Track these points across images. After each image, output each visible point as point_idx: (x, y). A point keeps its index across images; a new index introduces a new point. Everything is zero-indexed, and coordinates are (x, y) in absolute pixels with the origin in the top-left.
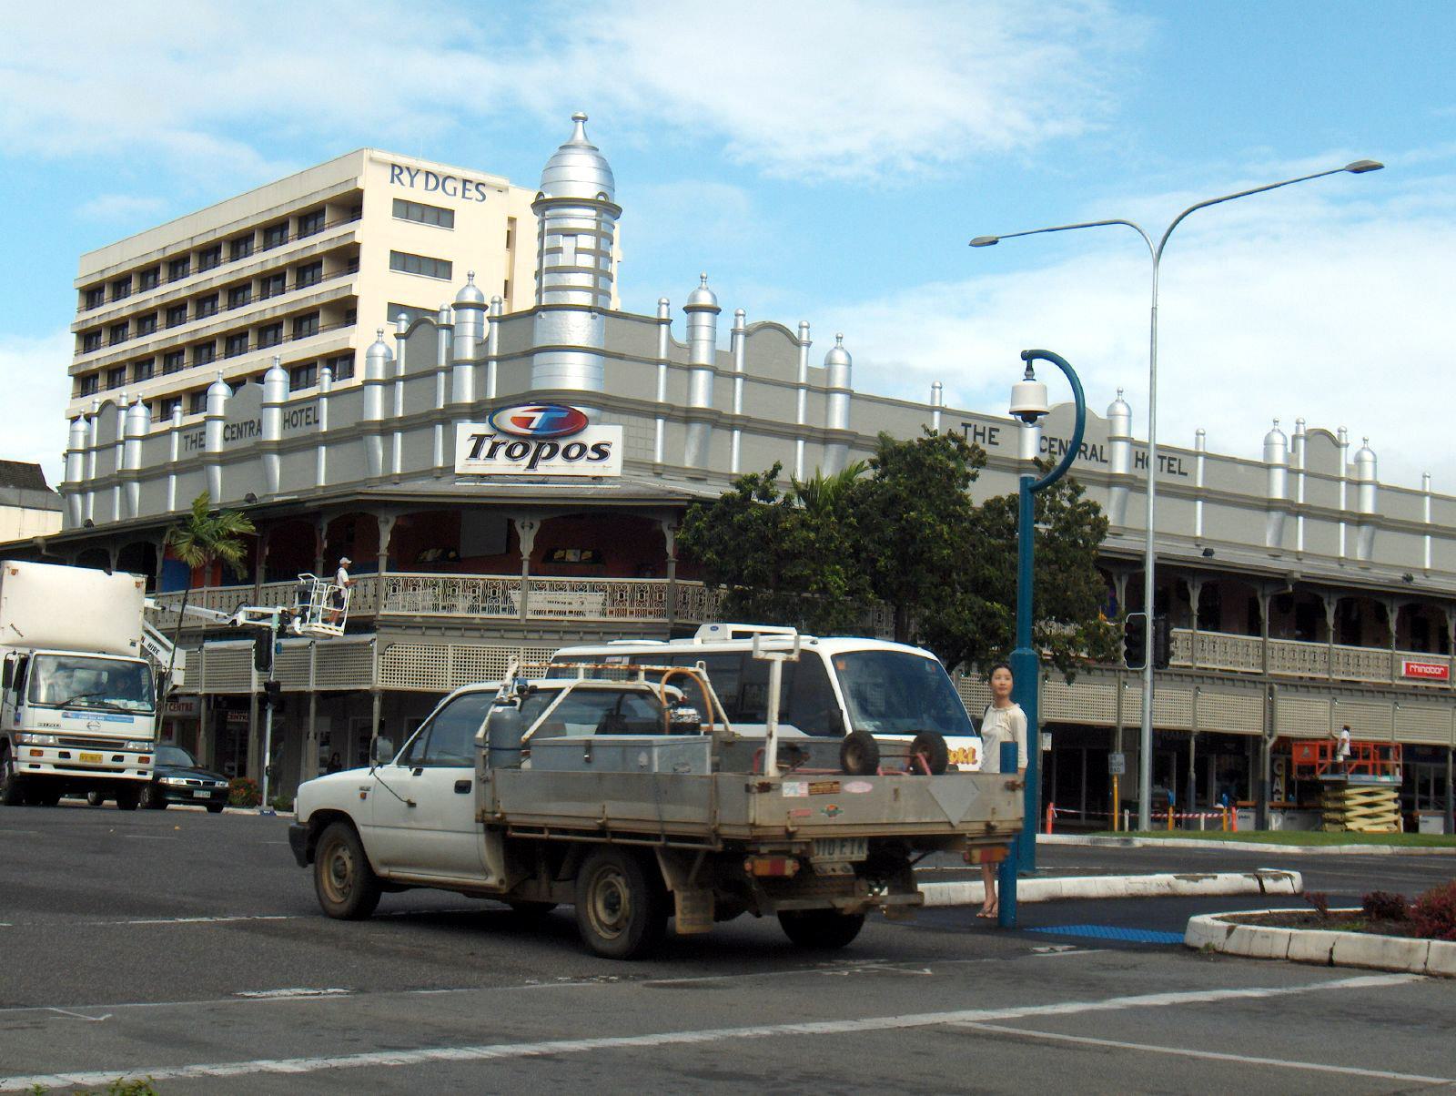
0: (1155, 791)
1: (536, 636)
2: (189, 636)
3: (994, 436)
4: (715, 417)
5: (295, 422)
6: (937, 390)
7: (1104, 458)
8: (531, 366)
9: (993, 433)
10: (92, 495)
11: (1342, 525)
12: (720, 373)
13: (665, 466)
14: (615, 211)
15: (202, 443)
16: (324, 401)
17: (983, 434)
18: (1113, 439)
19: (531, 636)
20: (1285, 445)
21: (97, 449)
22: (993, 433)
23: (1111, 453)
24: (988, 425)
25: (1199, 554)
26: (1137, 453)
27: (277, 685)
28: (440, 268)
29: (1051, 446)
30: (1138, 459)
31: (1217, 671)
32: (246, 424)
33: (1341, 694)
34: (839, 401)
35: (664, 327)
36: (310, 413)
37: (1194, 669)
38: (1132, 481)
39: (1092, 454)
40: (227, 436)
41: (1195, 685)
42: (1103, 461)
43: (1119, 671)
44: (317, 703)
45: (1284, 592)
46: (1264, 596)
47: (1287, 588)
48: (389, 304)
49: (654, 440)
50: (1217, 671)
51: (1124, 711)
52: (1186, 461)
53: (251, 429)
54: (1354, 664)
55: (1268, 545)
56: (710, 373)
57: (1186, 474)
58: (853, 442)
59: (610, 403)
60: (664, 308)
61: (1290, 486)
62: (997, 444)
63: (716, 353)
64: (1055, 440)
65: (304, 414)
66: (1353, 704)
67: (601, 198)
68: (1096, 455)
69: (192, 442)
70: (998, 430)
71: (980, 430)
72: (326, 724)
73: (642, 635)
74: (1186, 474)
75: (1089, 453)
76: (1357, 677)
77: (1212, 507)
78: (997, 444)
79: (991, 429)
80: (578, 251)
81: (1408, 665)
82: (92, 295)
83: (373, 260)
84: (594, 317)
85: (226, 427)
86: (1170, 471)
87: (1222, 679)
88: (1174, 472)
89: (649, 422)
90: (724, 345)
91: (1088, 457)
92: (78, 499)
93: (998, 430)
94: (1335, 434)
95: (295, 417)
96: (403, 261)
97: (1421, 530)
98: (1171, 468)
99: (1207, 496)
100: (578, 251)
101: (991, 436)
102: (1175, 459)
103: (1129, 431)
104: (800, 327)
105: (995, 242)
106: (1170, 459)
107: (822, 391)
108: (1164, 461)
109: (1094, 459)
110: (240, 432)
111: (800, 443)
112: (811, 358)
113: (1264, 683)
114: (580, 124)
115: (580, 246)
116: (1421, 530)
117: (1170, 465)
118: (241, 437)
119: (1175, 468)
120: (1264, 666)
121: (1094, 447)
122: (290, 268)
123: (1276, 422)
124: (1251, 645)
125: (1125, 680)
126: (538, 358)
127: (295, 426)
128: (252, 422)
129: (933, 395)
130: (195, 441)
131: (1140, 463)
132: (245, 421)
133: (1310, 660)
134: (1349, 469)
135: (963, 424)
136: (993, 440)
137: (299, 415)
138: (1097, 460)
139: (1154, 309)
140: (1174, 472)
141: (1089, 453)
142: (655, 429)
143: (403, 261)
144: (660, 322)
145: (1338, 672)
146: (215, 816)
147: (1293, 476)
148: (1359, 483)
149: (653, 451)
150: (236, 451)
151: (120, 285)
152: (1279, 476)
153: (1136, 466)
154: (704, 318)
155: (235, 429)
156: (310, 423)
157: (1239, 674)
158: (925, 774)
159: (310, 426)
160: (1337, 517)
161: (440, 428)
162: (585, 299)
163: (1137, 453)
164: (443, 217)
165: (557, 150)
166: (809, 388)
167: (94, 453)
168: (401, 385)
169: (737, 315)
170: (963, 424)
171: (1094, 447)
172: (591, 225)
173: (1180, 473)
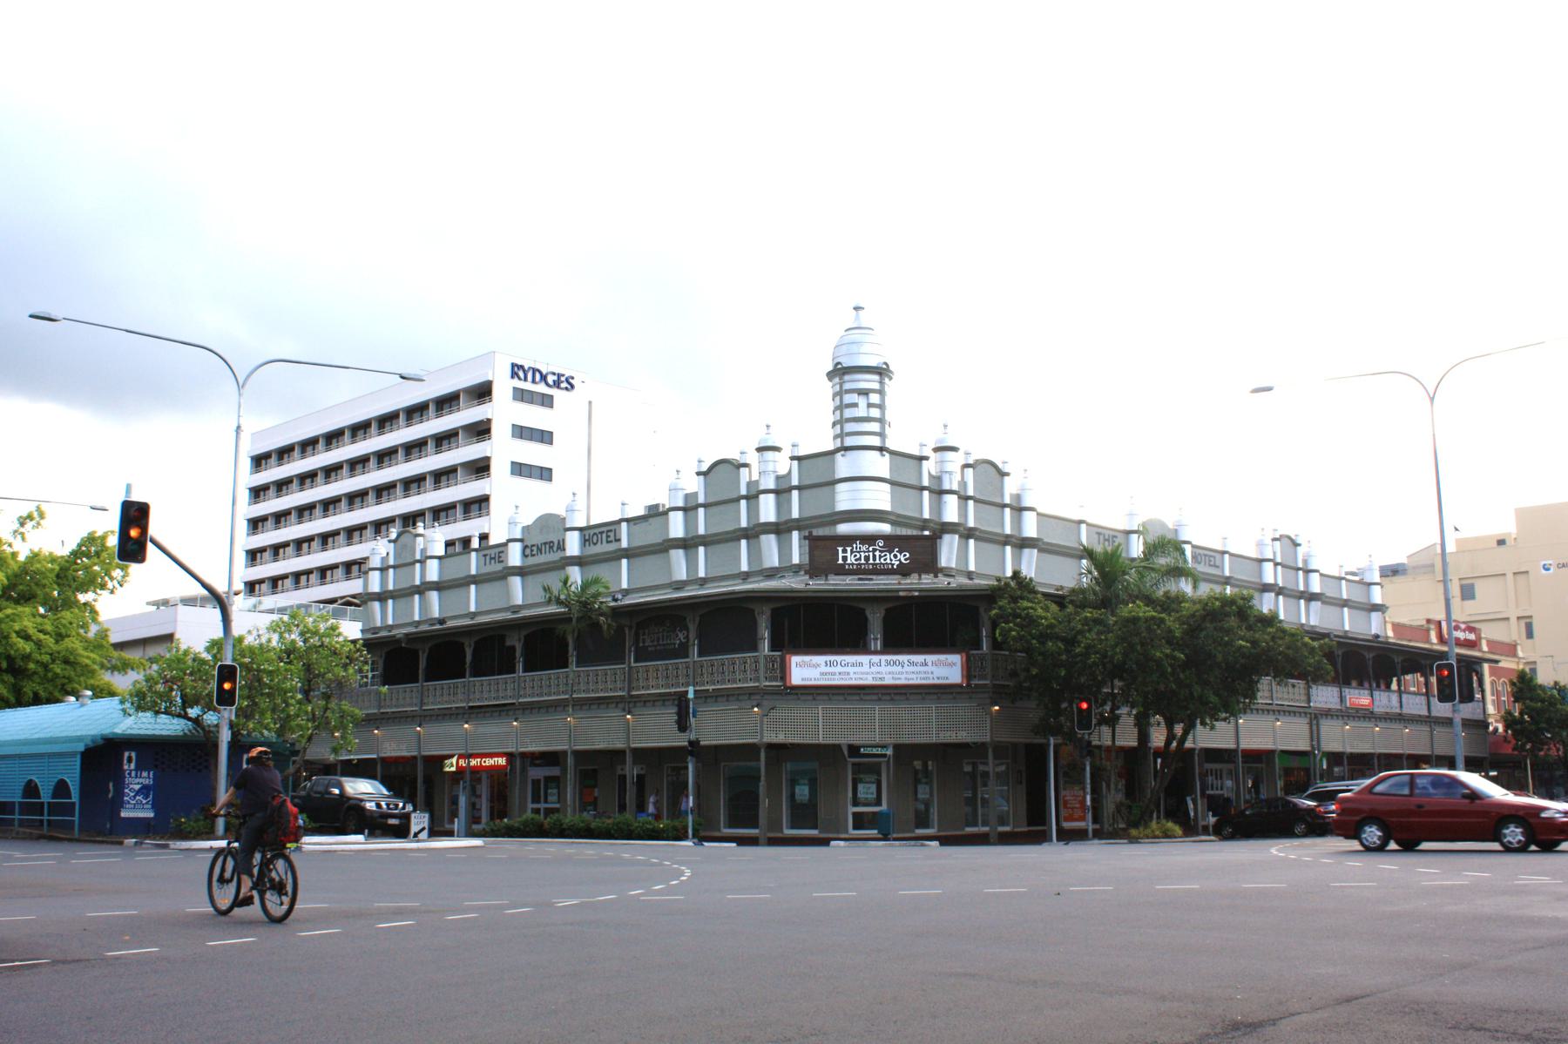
1: (888, 697)
2: (547, 707)
5: (595, 541)
8: (833, 493)
10: (390, 602)
13: (957, 570)
15: (501, 559)
16: (624, 525)
17: (494, 558)
19: (884, 697)
21: (394, 567)
24: (1111, 533)
27: (698, 742)
28: (545, 437)
32: (545, 543)
36: (612, 534)
40: (526, 554)
44: (766, 753)
48: (512, 463)
51: (1435, 746)
53: (551, 547)
65: (604, 535)
66: (722, 710)
69: (491, 559)
70: (503, 552)
71: (493, 556)
72: (344, 752)
81: (1350, 698)
82: (259, 461)
83: (500, 431)
85: (525, 547)
92: (376, 605)
94: (1293, 537)
95: (595, 537)
96: (521, 432)
100: (870, 405)
107: (1019, 509)
110: (540, 550)
112: (1010, 487)
115: (872, 401)
118: (541, 553)
120: (1309, 701)
122: (431, 439)
126: (840, 487)
127: (595, 544)
128: (552, 542)
130: (494, 558)
132: (545, 541)
133: (602, 681)
137: (599, 536)
139: (1434, 435)
143: (521, 432)
145: (579, 691)
146: (700, 847)
150: (529, 566)
151: (284, 453)
155: (535, 548)
156: (611, 542)
159: (610, 545)
161: (744, 543)
164: (547, 401)
167: (391, 571)
168: (701, 511)
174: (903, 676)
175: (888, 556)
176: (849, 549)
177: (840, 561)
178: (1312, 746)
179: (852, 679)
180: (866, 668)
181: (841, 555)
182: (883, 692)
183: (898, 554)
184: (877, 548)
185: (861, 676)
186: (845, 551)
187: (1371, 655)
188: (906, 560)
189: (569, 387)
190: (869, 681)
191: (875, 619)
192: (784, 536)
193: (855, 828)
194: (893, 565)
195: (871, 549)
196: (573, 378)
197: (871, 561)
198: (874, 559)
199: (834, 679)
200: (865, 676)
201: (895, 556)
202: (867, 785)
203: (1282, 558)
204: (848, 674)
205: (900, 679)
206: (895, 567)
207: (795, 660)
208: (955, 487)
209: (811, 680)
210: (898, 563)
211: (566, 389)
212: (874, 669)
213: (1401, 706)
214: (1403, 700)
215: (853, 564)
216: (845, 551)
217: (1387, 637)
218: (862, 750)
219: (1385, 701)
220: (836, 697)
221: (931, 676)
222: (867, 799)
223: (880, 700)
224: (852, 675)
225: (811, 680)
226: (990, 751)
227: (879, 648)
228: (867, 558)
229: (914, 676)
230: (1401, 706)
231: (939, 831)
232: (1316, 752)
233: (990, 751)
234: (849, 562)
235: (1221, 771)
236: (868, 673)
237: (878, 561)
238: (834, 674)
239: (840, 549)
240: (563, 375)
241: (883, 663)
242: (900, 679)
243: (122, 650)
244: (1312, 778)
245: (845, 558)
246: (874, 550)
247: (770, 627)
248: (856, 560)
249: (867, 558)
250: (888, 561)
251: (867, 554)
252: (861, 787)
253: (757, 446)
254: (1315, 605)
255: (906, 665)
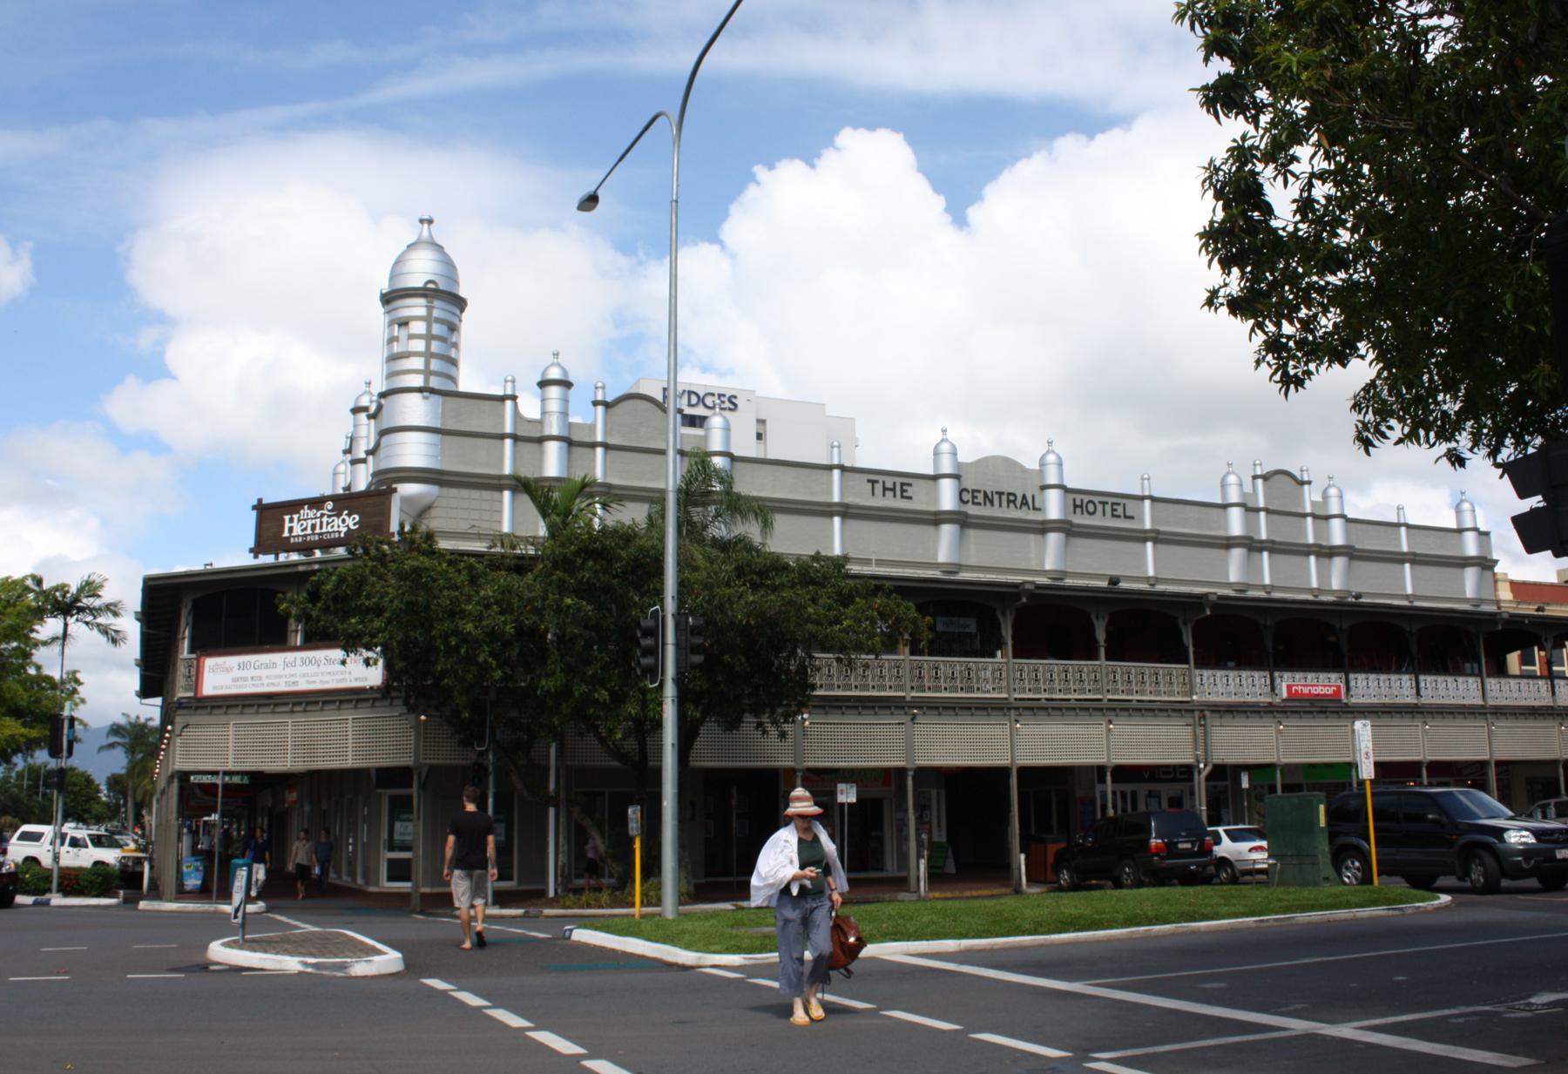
0: (1554, 816)
3: (906, 491)
4: (962, 517)
6: (1146, 482)
7: (1127, 514)
9: (905, 488)
11: (1407, 566)
12: (1249, 509)
14: (460, 303)
18: (1044, 488)
20: (1241, 485)
22: (905, 488)
23: (1043, 501)
24: (1086, 498)
25: (1104, 584)
26: (1074, 500)
29: (974, 497)
30: (1075, 506)
31: (1134, 702)
33: (1117, 715)
34: (1336, 524)
35: (1306, 487)
37: (1105, 701)
38: (1483, 561)
39: (1022, 504)
41: (1107, 719)
42: (1034, 508)
43: (1009, 709)
45: (1202, 616)
46: (1185, 623)
47: (1204, 611)
49: (500, 511)
50: (1043, 701)
52: (1131, 507)
54: (1261, 685)
55: (1048, 567)
56: (565, 445)
57: (1132, 518)
58: (1069, 530)
59: (446, 478)
60: (1305, 474)
61: (1250, 523)
62: (910, 498)
63: (1244, 495)
64: (979, 491)
67: (431, 286)
68: (1027, 504)
70: (910, 485)
73: (209, 710)
74: (1132, 518)
75: (1018, 502)
76: (998, 693)
77: (1419, 568)
78: (910, 498)
79: (902, 484)
80: (411, 337)
84: (425, 398)
86: (1113, 516)
87: (1140, 710)
88: (1119, 516)
89: (495, 494)
90: (1248, 488)
91: (1018, 506)
93: (910, 485)
97: (1399, 559)
98: (976, 500)
99: (1158, 537)
100: (411, 337)
101: (903, 491)
102: (1118, 504)
103: (1342, 506)
104: (1302, 471)
105: (409, 246)
106: (1113, 504)
107: (1323, 518)
108: (876, 485)
109: (1025, 508)
111: (1312, 558)
113: (1193, 711)
114: (426, 226)
116: (1399, 559)
117: (1113, 510)
119: (1120, 511)
121: (1024, 497)
123: (1462, 493)
124: (1174, 673)
125: (1018, 718)
129: (1398, 515)
131: (1078, 510)
134: (1313, 503)
135: (869, 481)
136: (905, 494)
138: (895, 496)
140: (1119, 516)
141: (1018, 502)
142: (501, 502)
144: (502, 399)
147: (1323, 522)
148: (1328, 518)
149: (500, 522)
152: (1235, 515)
153: (1075, 512)
154: (554, 391)
157: (1043, 701)
158: (87, 847)
160: (1304, 551)
162: (417, 381)
163: (1074, 500)
165: (405, 248)
166: (516, 438)
169: (596, 388)
170: (869, 481)
171: (1024, 497)
172: (422, 312)
173: (1126, 517)
174: (317, 679)
175: (336, 523)
176: (296, 517)
177: (286, 534)
178: (1197, 757)
179: (263, 685)
180: (279, 670)
181: (287, 525)
182: (324, 699)
183: (347, 518)
184: (326, 512)
185: (273, 681)
186: (291, 520)
187: (1345, 626)
188: (355, 524)
189: (732, 407)
190: (281, 687)
191: (290, 602)
192: (1255, 555)
193: (391, 878)
194: (339, 532)
195: (318, 515)
196: (735, 397)
197: (318, 531)
198: (321, 528)
199: (246, 686)
200: (278, 680)
201: (344, 521)
202: (405, 824)
203: (1266, 503)
204: (261, 678)
205: (314, 682)
206: (342, 535)
207: (210, 663)
208: (555, 431)
209: (222, 688)
210: (346, 529)
211: (730, 409)
212: (289, 671)
213: (1418, 693)
214: (1422, 685)
215: (298, 536)
216: (291, 520)
217: (1497, 602)
218: (192, 778)
219: (1503, 692)
220: (995, 713)
221: (348, 677)
222: (403, 841)
223: (292, 712)
224: (265, 681)
225: (222, 688)
226: (1109, 775)
227: (298, 643)
228: (314, 527)
229: (329, 678)
230: (1418, 693)
231: (520, 883)
232: (1202, 766)
233: (1109, 775)
234: (294, 534)
235: (1134, 794)
236: (280, 677)
237: (324, 530)
238: (245, 679)
239: (287, 518)
240: (724, 395)
241: (298, 662)
242: (314, 682)
243: (1416, 704)
244: (1197, 802)
245: (291, 529)
246: (322, 515)
247: (191, 623)
248: (303, 530)
249: (314, 527)
250: (336, 529)
251: (314, 521)
252: (398, 825)
253: (352, 406)
254: (1339, 563)
255: (322, 665)
